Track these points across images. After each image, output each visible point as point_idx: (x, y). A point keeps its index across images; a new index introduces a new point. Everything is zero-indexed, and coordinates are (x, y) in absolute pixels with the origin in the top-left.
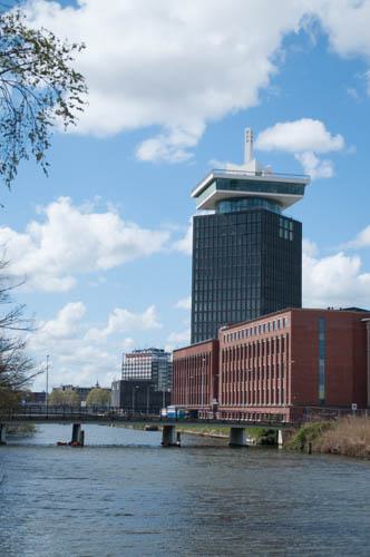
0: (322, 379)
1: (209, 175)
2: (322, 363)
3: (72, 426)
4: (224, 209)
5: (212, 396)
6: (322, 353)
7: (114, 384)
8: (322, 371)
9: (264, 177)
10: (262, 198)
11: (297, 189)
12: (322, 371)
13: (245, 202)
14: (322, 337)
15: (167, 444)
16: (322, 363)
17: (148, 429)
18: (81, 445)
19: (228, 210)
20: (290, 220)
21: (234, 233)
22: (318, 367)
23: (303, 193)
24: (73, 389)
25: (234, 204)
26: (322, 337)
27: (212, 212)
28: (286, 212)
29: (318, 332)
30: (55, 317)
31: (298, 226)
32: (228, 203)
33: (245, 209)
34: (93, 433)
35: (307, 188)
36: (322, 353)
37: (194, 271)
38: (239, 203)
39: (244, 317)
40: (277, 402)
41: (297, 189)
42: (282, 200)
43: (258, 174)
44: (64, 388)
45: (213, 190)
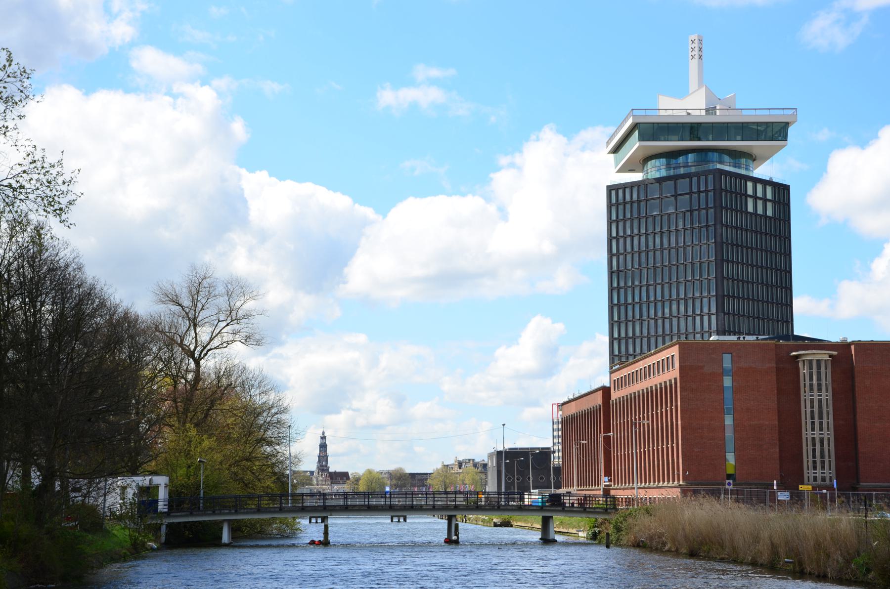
0: (730, 445)
1: (625, 120)
2: (729, 421)
3: (539, 519)
4: (655, 170)
5: (602, 472)
6: (729, 405)
7: (490, 456)
8: (729, 434)
9: (720, 116)
10: (721, 151)
11: (776, 131)
12: (729, 434)
13: (691, 157)
14: (728, 382)
15: (547, 541)
16: (729, 421)
17: (496, 525)
18: (456, 542)
19: (664, 173)
20: (765, 183)
21: (672, 210)
22: (723, 428)
23: (785, 138)
24: (475, 465)
25: (673, 161)
26: (728, 382)
27: (637, 177)
28: (761, 171)
29: (722, 375)
30: (513, 340)
31: (782, 191)
32: (663, 161)
33: (693, 170)
34: (472, 528)
35: (791, 131)
36: (729, 405)
37: (613, 273)
38: (681, 159)
39: (645, 347)
40: (668, 481)
41: (776, 131)
42: (755, 152)
43: (710, 110)
44: (460, 464)
45: (634, 145)
